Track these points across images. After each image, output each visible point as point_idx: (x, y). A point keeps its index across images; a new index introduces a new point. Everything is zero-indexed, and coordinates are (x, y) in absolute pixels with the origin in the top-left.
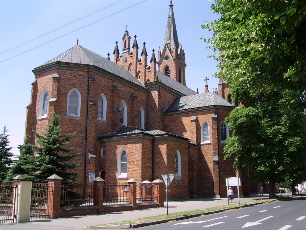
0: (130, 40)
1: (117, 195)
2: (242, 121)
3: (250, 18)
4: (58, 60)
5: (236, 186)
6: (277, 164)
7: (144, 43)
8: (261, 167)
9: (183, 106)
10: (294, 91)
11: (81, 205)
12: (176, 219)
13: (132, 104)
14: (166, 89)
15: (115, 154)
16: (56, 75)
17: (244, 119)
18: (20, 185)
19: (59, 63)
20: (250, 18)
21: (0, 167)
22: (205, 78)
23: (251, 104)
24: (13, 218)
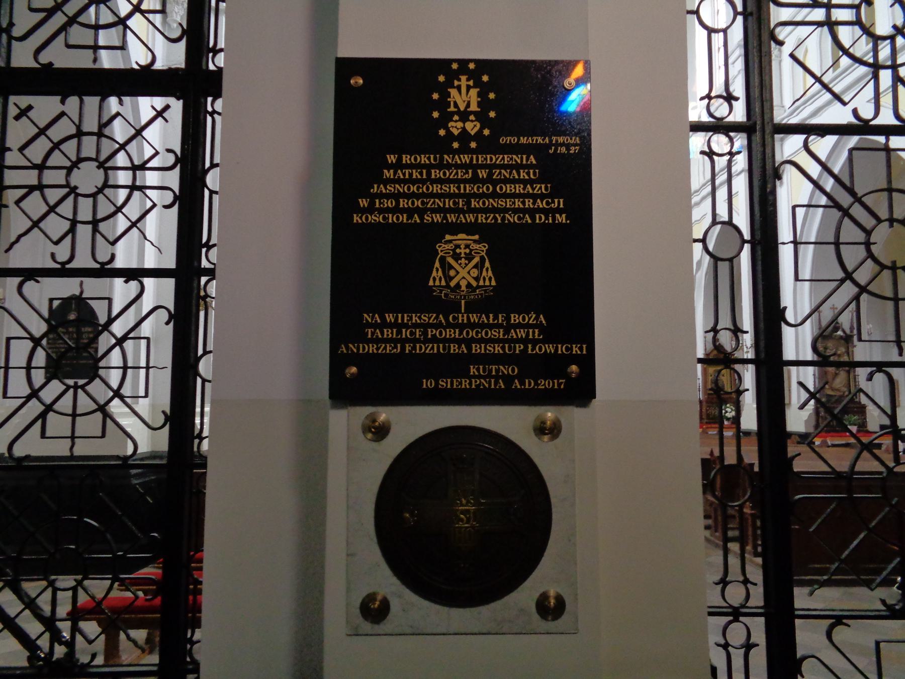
0: (475, 128)
1: (864, 405)
2: (550, 105)
3: (55, 580)
4: (789, 159)
5: (4, 453)
6: (466, 170)
7: (831, 306)
8: (862, 416)
9: (790, 170)
10: (39, 652)
11: (550, 215)
12: (486, 318)
13: (573, 89)
14: (714, 13)
15: (488, 259)
16: (756, 469)
17: (375, 326)
18: (131, 471)
19: (111, 263)
20: (55, 580)
21: (174, 1)
22: (835, 307)
23: (582, 79)
24: (723, 25)
